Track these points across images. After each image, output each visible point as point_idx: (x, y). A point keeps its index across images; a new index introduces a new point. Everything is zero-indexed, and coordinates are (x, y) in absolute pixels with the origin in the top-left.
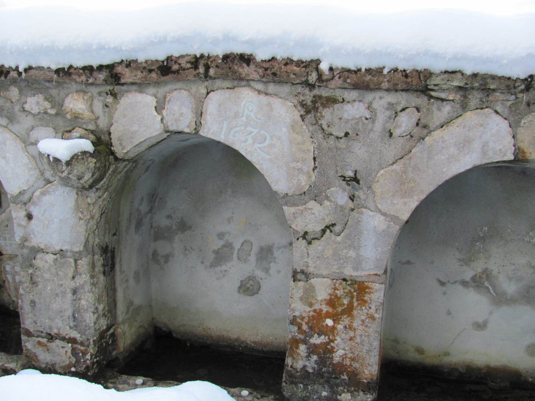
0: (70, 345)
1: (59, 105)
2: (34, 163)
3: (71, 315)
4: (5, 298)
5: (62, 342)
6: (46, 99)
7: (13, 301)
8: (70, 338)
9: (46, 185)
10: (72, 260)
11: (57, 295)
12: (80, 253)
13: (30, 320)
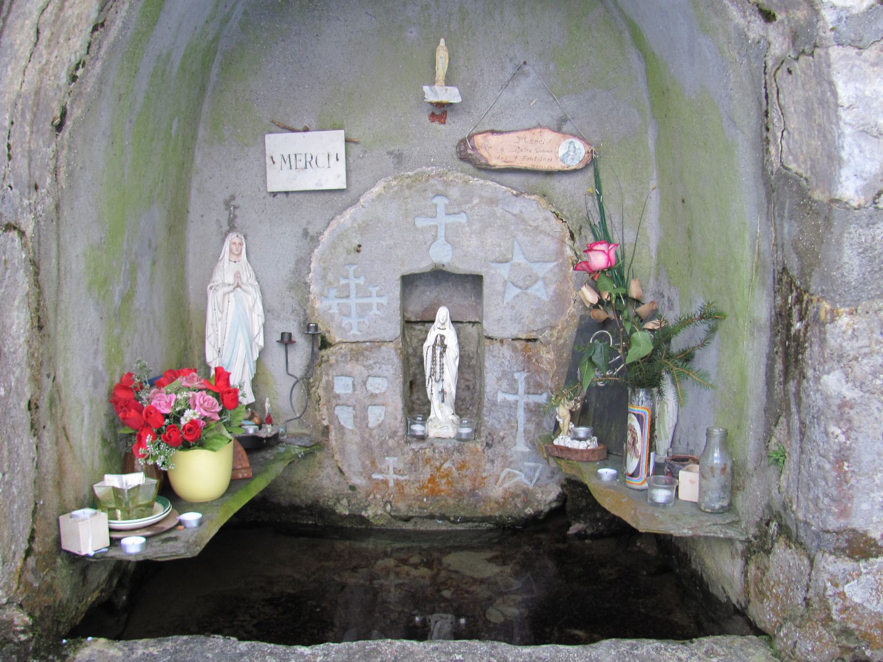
4: (326, 482)
7: (353, 488)
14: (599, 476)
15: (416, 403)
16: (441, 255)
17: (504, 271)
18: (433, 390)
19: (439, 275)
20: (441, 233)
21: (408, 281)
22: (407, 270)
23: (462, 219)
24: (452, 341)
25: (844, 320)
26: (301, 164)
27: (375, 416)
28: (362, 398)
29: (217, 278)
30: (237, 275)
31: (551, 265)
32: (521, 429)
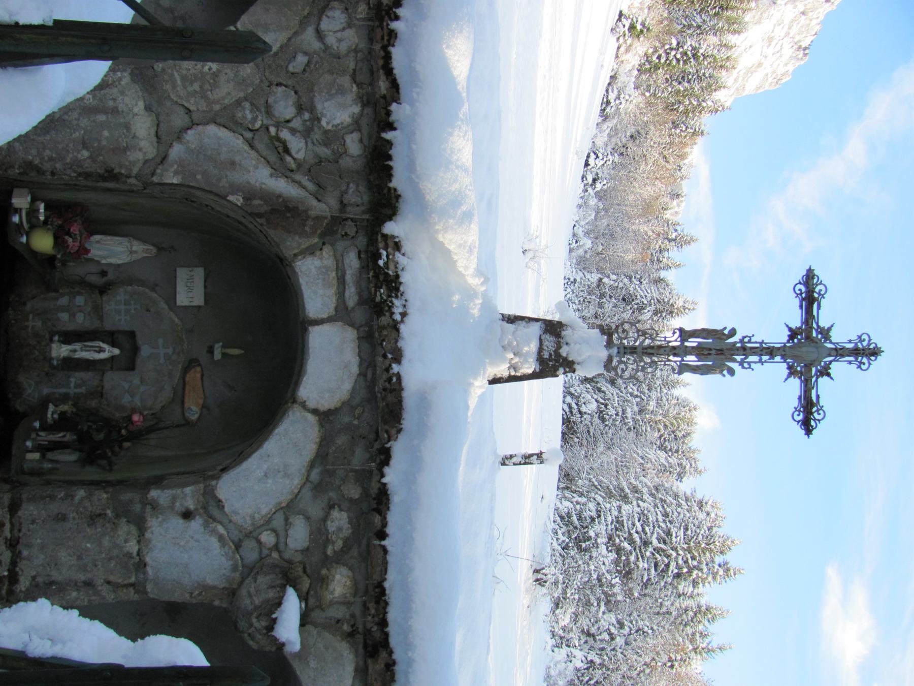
0: (6, 573)
1: (339, 559)
2: (262, 522)
3: (53, 578)
5: (8, 560)
6: (346, 541)
7: (25, 304)
8: (16, 574)
9: (233, 543)
10: (133, 580)
11: (80, 558)
12: (145, 592)
13: (35, 513)
14: (36, 420)
15: (69, 337)
16: (145, 351)
17: (137, 381)
18: (77, 346)
19: (135, 349)
20: (155, 351)
21: (132, 334)
22: (139, 335)
23: (162, 361)
24: (102, 356)
25: (105, 496)
26: (189, 284)
27: (64, 316)
28: (74, 311)
29: (135, 243)
30: (136, 252)
31: (139, 404)
32: (55, 390)
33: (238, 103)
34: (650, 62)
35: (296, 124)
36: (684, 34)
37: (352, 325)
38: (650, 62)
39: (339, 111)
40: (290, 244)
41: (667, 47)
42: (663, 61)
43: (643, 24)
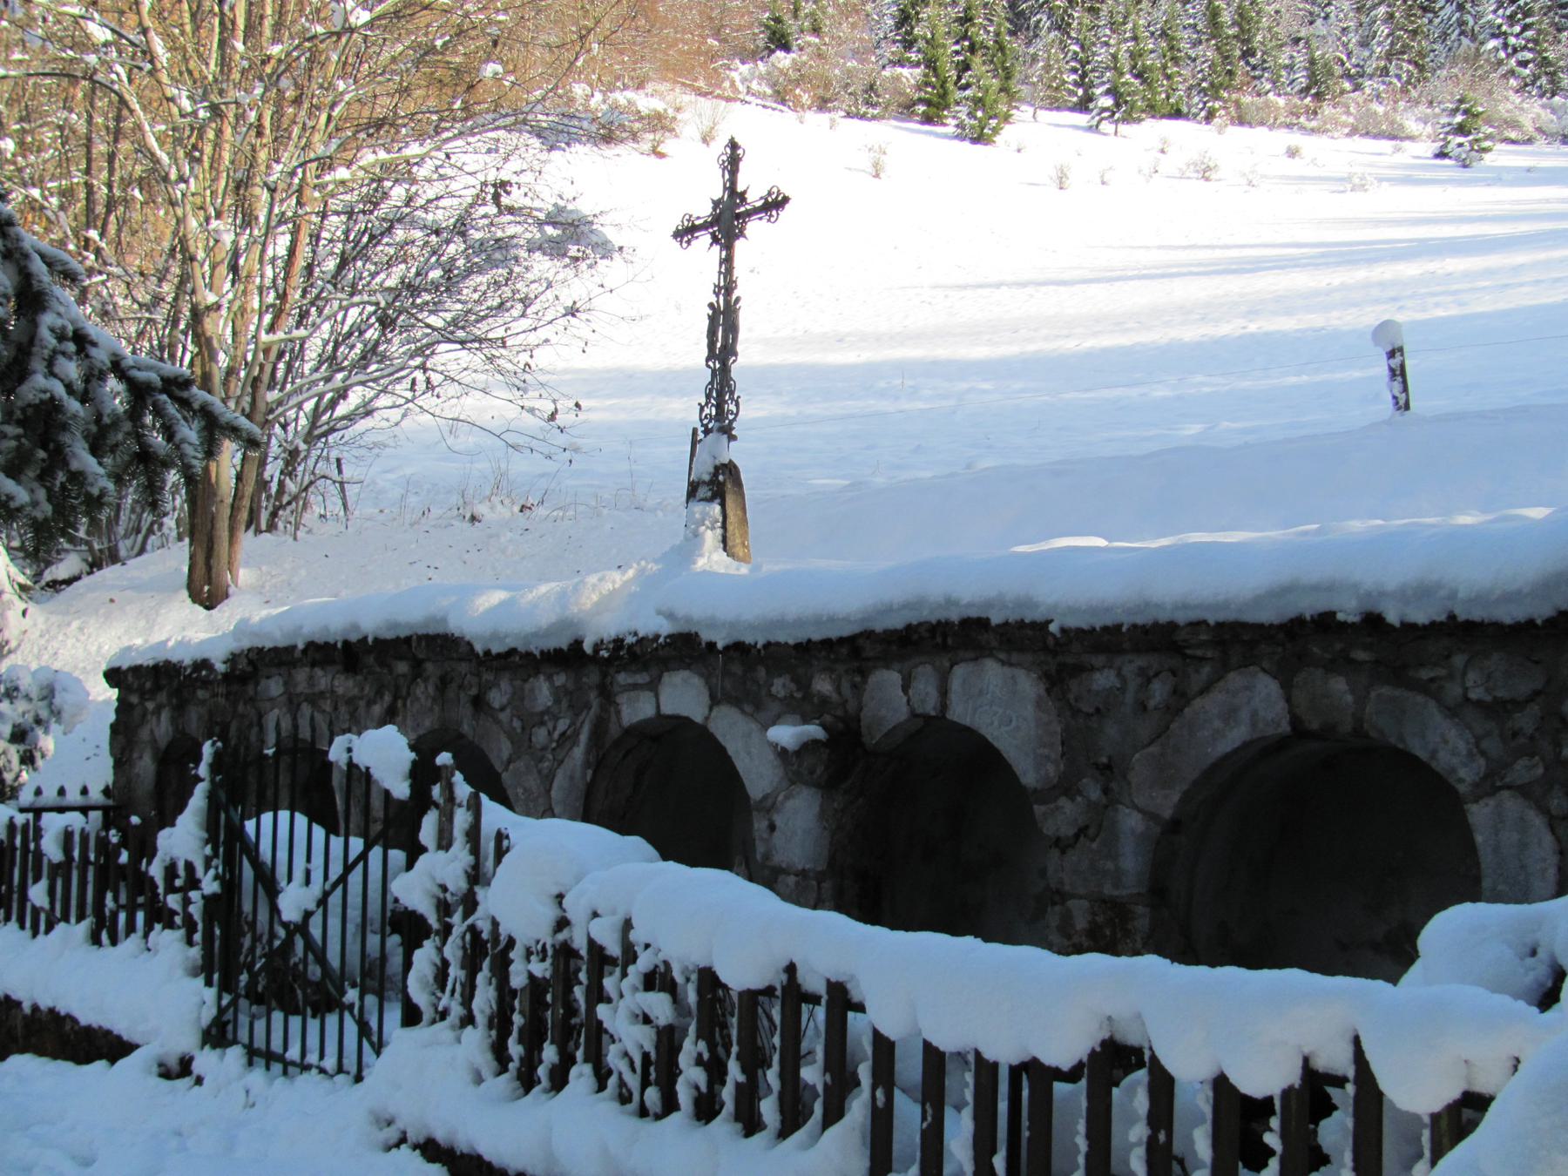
33: (539, 772)
34: (1536, 78)
35: (550, 725)
36: (1477, 29)
37: (660, 677)
38: (1536, 78)
39: (542, 692)
40: (614, 731)
41: (1502, 55)
42: (1530, 56)
43: (1454, 112)
